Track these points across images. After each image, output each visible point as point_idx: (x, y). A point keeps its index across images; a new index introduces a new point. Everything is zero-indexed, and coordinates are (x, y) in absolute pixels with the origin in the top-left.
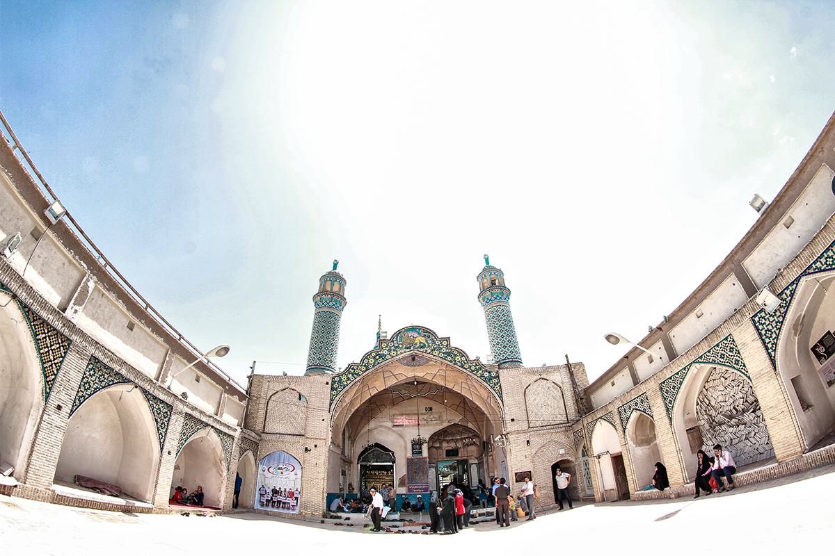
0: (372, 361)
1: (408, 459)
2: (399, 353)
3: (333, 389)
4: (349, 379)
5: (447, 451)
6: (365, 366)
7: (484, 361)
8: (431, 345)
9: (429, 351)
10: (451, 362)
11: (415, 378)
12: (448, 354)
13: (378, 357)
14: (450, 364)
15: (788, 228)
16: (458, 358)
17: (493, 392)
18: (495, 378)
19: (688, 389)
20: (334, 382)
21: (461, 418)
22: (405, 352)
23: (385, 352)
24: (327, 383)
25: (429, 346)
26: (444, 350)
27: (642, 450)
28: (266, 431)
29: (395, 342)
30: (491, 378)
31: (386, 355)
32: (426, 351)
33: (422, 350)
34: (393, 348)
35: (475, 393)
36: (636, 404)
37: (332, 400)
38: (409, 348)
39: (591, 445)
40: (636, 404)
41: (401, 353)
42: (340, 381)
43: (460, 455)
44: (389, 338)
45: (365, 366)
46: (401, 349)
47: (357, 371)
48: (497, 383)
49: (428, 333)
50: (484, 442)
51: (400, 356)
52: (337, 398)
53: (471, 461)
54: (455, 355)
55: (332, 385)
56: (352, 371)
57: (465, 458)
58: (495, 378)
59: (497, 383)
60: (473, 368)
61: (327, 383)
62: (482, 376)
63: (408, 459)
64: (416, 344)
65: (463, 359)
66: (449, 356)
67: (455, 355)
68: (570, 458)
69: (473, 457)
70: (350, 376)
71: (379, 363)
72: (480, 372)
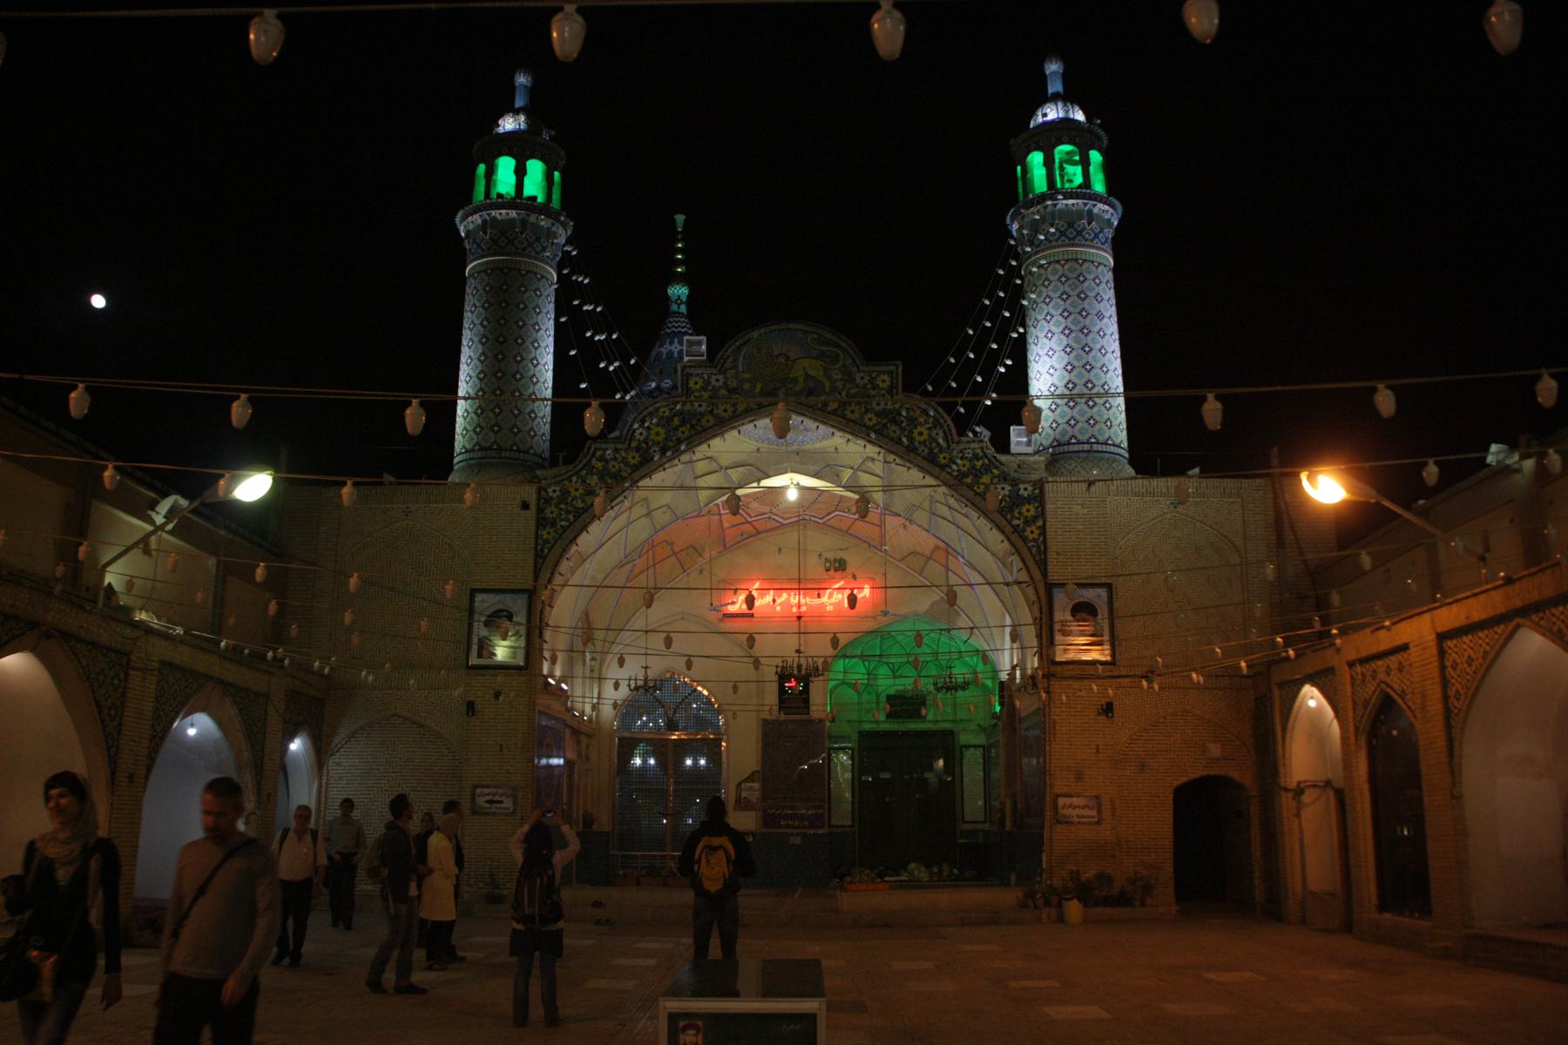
1: (765, 722)
2: (741, 408)
3: (541, 522)
6: (638, 449)
8: (839, 385)
9: (833, 406)
15: (646, 499)
18: (1028, 500)
19: (1288, 735)
24: (525, 506)
27: (820, 1002)
28: (658, 527)
29: (731, 373)
31: (702, 415)
32: (825, 404)
36: (1388, 671)
39: (1284, 748)
40: (1388, 671)
45: (638, 449)
48: (1035, 519)
50: (1002, 683)
55: (540, 510)
56: (599, 465)
57: (947, 726)
58: (1028, 500)
59: (1035, 519)
63: (765, 722)
64: (795, 380)
68: (1234, 774)
70: (594, 480)
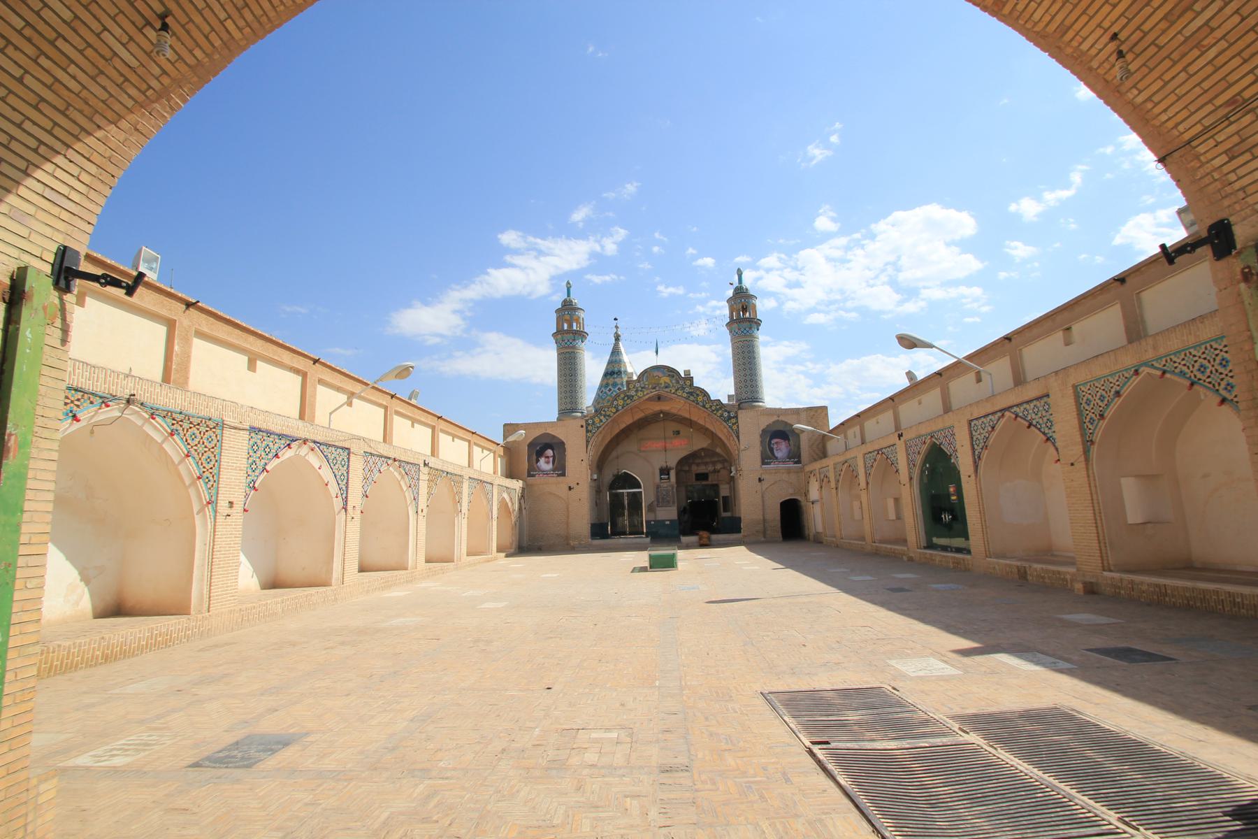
0: (621, 402)
2: (645, 393)
3: (588, 431)
4: (601, 421)
7: (725, 401)
9: (673, 391)
10: (693, 401)
11: (661, 412)
12: (691, 394)
13: (626, 398)
14: (693, 403)
16: (700, 398)
17: (731, 431)
20: (588, 424)
22: (652, 392)
23: (633, 393)
24: (582, 426)
25: (673, 386)
26: (687, 390)
30: (730, 418)
33: (667, 390)
34: (640, 389)
35: (721, 430)
37: (588, 442)
38: (654, 388)
41: (648, 394)
42: (593, 423)
43: (710, 479)
44: (635, 378)
46: (648, 389)
47: (608, 413)
48: (735, 423)
49: (671, 372)
51: (647, 397)
52: (593, 439)
54: (698, 395)
55: (587, 428)
59: (735, 423)
60: (713, 408)
61: (582, 426)
62: (722, 415)
65: (705, 399)
66: (692, 395)
67: (698, 395)
70: (602, 417)
71: (627, 404)
72: (720, 412)
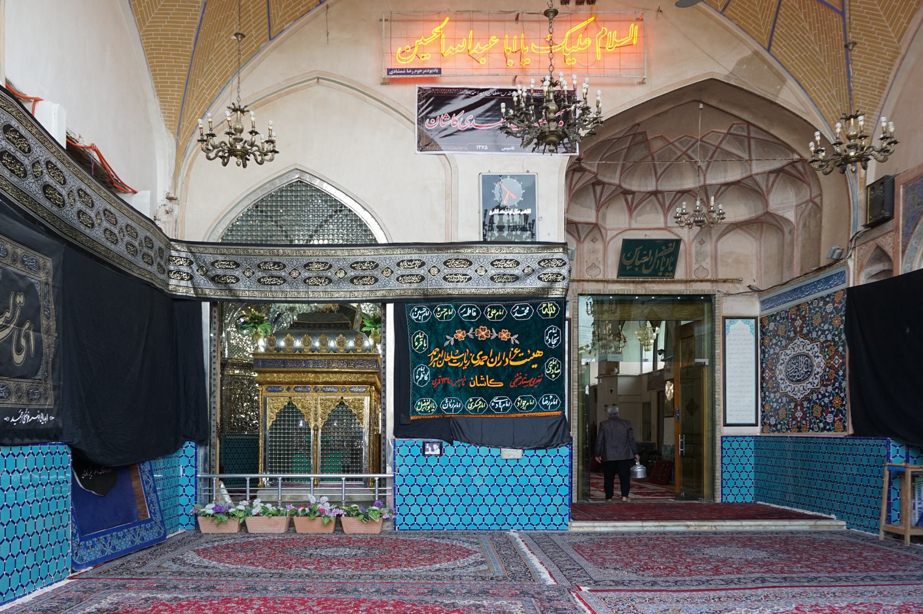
5: (629, 245)
21: (748, 53)
53: (726, 307)
57: (706, 288)
69: (742, 288)
